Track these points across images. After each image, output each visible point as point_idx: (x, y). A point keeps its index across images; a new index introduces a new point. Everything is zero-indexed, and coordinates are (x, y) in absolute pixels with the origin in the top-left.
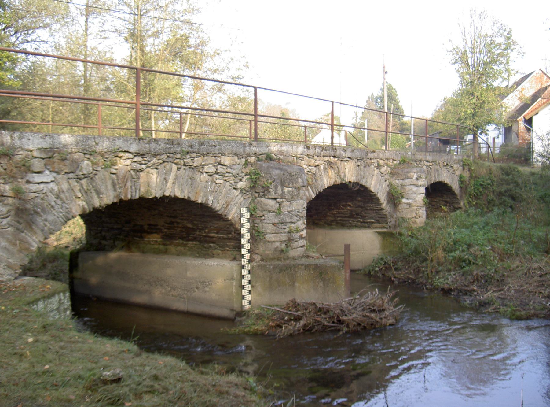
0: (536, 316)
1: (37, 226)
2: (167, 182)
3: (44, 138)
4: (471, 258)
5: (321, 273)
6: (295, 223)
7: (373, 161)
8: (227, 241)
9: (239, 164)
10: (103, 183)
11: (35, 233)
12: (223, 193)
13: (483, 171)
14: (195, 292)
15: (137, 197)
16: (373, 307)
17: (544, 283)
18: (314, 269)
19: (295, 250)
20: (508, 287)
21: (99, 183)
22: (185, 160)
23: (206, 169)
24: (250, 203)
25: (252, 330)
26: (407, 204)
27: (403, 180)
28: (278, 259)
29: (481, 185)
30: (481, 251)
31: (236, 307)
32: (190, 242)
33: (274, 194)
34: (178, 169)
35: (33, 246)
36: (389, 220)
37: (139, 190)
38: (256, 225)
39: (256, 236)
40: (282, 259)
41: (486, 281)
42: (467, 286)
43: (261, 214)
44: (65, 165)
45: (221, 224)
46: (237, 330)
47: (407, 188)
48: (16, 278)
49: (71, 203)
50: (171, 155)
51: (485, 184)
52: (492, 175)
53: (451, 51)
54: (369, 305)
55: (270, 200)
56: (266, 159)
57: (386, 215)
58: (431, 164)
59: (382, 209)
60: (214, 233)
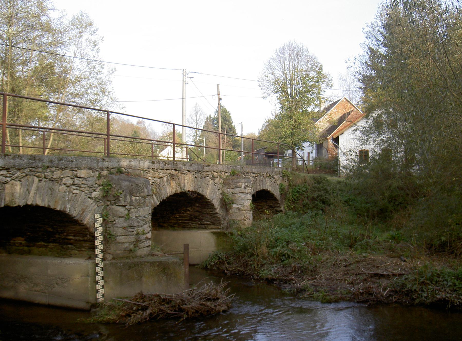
2: (29, 193)
4: (289, 253)
5: (164, 269)
6: (141, 226)
13: (299, 181)
18: (158, 266)
22: (46, 174)
23: (64, 181)
24: (103, 210)
26: (237, 208)
27: (233, 188)
28: (128, 258)
29: (298, 192)
30: (297, 246)
31: (92, 300)
33: (123, 202)
34: (40, 181)
36: (222, 222)
37: (5, 199)
38: (108, 229)
40: (131, 258)
41: (301, 272)
42: (287, 276)
43: (113, 219)
45: (78, 228)
46: (92, 320)
47: (237, 195)
50: (33, 169)
51: (301, 191)
54: (205, 295)
55: (120, 208)
56: (117, 172)
58: (256, 175)
59: (217, 213)
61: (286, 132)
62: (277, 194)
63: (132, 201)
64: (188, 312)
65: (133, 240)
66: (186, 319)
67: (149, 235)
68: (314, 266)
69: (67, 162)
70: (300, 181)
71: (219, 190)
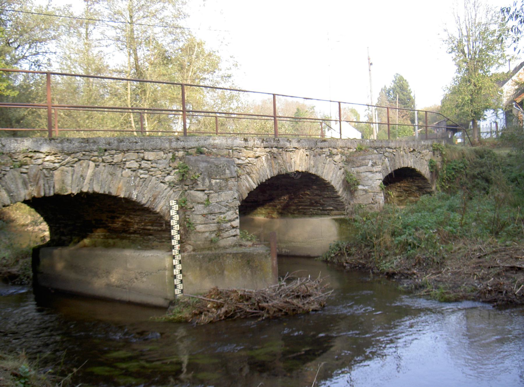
0: (465, 298)
2: (84, 179)
4: (415, 242)
5: (248, 261)
6: (224, 213)
7: (324, 150)
8: (161, 233)
9: (165, 159)
10: (13, 182)
12: (149, 187)
13: (456, 155)
14: (134, 282)
15: (52, 194)
16: (298, 293)
17: (481, 264)
18: (242, 257)
20: (446, 269)
22: (104, 157)
23: (128, 164)
24: (181, 196)
25: (176, 318)
26: (364, 190)
27: (358, 167)
28: (209, 249)
29: (453, 169)
30: (425, 234)
31: (169, 295)
32: (132, 235)
33: (201, 186)
34: (97, 166)
36: (346, 207)
37: (54, 187)
38: (187, 217)
39: (187, 228)
40: (213, 249)
42: (408, 270)
43: (191, 206)
45: (147, 217)
46: (164, 319)
50: (87, 153)
52: (465, 159)
53: (447, 41)
54: (293, 291)
55: (199, 192)
56: (196, 153)
57: (342, 202)
58: (395, 150)
59: (339, 197)
60: (149, 225)
61: (463, 99)
62: (424, 170)
63: (211, 184)
64: (268, 311)
65: (215, 229)
66: (266, 318)
67: (236, 223)
68: (441, 257)
69: (130, 143)
70: (457, 155)
71: (340, 169)
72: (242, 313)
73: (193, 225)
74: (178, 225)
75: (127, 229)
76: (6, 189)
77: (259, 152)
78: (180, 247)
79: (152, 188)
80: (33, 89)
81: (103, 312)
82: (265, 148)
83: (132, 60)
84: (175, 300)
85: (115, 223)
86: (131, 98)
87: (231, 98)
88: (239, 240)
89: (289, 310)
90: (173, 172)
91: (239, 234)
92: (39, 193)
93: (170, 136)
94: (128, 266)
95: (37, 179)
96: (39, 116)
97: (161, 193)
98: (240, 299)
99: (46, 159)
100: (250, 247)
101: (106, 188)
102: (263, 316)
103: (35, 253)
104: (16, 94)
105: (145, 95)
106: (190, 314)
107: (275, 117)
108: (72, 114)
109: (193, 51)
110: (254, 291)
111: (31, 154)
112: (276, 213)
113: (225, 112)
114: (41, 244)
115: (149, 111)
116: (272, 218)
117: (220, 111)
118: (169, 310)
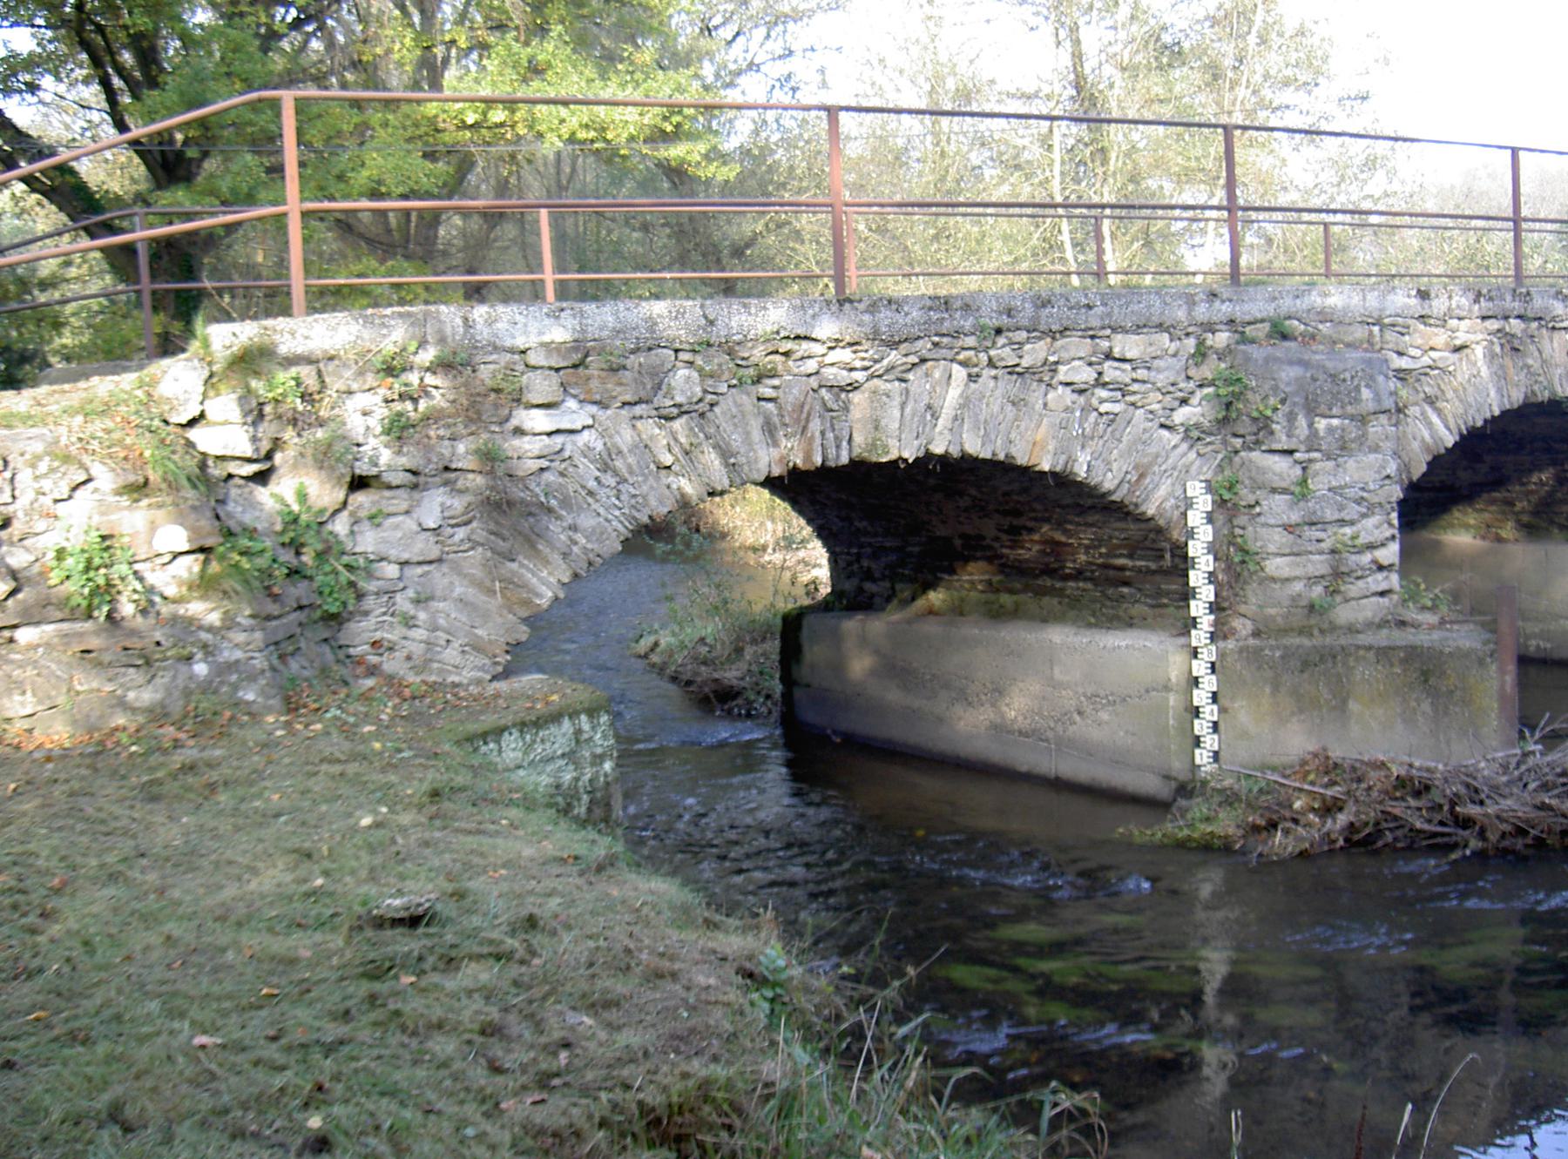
1: (550, 543)
2: (935, 417)
3: (558, 317)
5: (1424, 672)
6: (1352, 523)
8: (1158, 578)
9: (1174, 355)
11: (547, 562)
12: (1124, 439)
15: (844, 460)
18: (1405, 661)
19: (1353, 603)
21: (726, 426)
22: (992, 353)
23: (1063, 373)
28: (1304, 631)
31: (1178, 767)
32: (1071, 584)
33: (1284, 438)
34: (973, 378)
35: (539, 595)
37: (850, 441)
38: (1238, 531)
39: (1236, 566)
40: (1316, 632)
43: (1251, 499)
44: (621, 384)
45: (1118, 531)
46: (1159, 835)
48: (494, 678)
49: (645, 481)
50: (945, 340)
55: (1276, 458)
56: (1269, 336)
60: (1121, 556)
63: (1314, 433)
65: (1324, 569)
69: (1070, 308)
72: (1399, 833)
73: (1257, 558)
74: (1211, 558)
75: (1056, 566)
76: (716, 447)
77: (1465, 331)
78: (1216, 624)
79: (1135, 443)
80: (777, 157)
81: (981, 807)
82: (1484, 318)
83: (1065, 59)
84: (1193, 780)
85: (1023, 548)
86: (1062, 173)
87: (1371, 164)
88: (1395, 606)
89: (1550, 831)
90: (1199, 394)
91: (1397, 587)
92: (808, 456)
93: (1190, 285)
94: (1058, 674)
95: (804, 416)
96: (797, 235)
97: (1160, 460)
98: (1395, 788)
99: (828, 360)
100: (1430, 629)
101: (999, 442)
102: (1466, 846)
103: (792, 627)
104: (732, 175)
105: (1105, 162)
106: (1238, 826)
107: (1517, 220)
108: (890, 226)
109: (1251, 22)
110: (1441, 767)
111: (788, 345)
112: (1510, 524)
113: (1351, 207)
114: (807, 602)
115: (1117, 212)
116: (1499, 539)
117: (1332, 207)
118: (1174, 810)
